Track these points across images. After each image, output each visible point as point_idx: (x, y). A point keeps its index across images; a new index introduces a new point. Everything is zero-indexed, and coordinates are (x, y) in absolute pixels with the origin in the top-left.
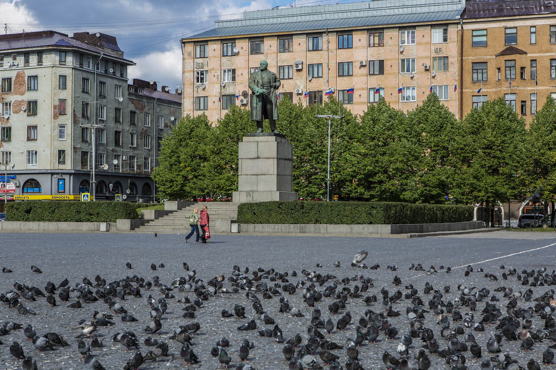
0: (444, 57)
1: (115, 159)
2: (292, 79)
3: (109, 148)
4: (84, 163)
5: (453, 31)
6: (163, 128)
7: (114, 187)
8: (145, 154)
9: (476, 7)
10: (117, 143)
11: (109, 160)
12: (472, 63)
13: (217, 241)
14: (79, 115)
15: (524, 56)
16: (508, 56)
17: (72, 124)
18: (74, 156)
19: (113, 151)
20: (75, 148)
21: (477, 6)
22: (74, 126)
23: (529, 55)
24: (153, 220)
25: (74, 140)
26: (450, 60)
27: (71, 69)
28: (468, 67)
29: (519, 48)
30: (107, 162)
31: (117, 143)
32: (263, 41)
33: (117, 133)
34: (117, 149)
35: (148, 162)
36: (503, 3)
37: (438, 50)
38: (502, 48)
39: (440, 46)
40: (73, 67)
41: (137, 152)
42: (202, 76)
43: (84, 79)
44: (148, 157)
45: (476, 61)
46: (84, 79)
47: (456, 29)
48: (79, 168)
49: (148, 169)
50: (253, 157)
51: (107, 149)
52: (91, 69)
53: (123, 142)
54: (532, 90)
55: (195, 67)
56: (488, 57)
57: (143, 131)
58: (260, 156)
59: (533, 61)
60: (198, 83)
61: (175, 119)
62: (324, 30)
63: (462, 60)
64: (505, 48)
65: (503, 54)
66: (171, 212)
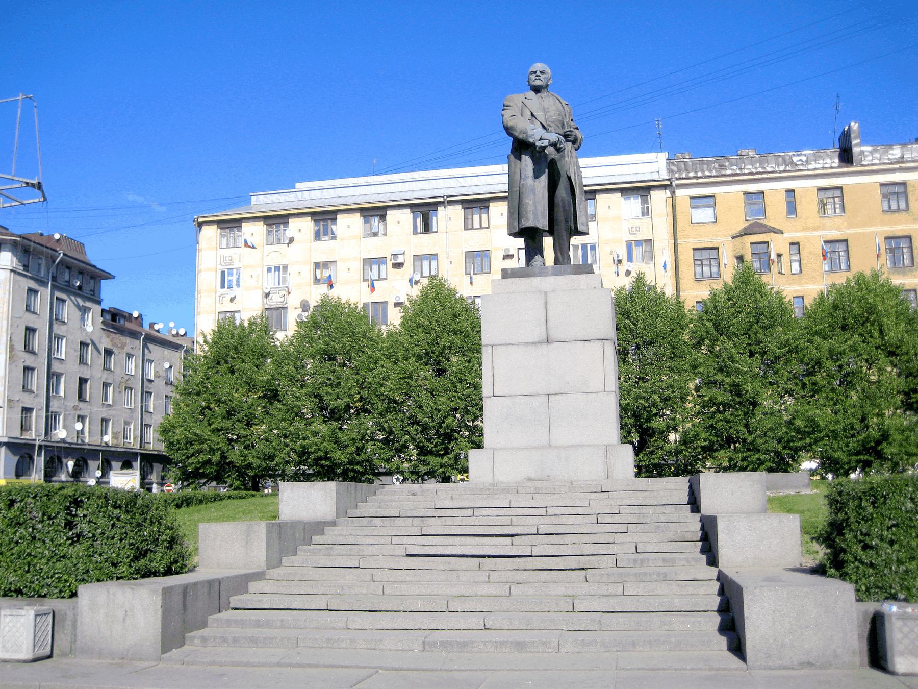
0: (645, 241)
1: (78, 421)
2: (386, 279)
3: (68, 404)
4: (24, 428)
5: (658, 197)
6: (152, 378)
7: (75, 465)
8: (125, 416)
9: (683, 166)
10: (81, 397)
11: (68, 423)
12: (694, 249)
13: (493, 628)
14: (20, 346)
15: (780, 235)
16: (756, 235)
17: (6, 361)
18: (8, 413)
19: (75, 408)
20: (9, 401)
21: (685, 165)
22: (10, 364)
23: (786, 235)
24: (258, 576)
25: (9, 387)
26: (657, 245)
27: (9, 271)
28: (687, 257)
29: (769, 224)
30: (65, 427)
31: (81, 397)
32: (336, 219)
33: (82, 381)
34: (81, 405)
35: (130, 429)
36: (726, 160)
37: (634, 229)
38: (742, 225)
39: (637, 223)
40: (11, 268)
41: (114, 412)
42: (230, 278)
43: (30, 290)
44: (130, 420)
45: (700, 247)
46: (30, 290)
47: (664, 196)
48: (16, 433)
49: (130, 439)
50: (531, 340)
51: (66, 406)
52: (42, 276)
53: (92, 395)
54: (795, 291)
55: (219, 263)
56: (722, 239)
57: (123, 380)
58: (553, 335)
59: (795, 244)
60: (223, 290)
61: (171, 367)
62: (442, 199)
63: (675, 245)
64: (747, 224)
65: (746, 232)
66: (318, 527)
